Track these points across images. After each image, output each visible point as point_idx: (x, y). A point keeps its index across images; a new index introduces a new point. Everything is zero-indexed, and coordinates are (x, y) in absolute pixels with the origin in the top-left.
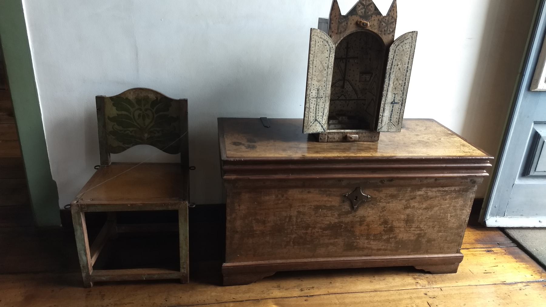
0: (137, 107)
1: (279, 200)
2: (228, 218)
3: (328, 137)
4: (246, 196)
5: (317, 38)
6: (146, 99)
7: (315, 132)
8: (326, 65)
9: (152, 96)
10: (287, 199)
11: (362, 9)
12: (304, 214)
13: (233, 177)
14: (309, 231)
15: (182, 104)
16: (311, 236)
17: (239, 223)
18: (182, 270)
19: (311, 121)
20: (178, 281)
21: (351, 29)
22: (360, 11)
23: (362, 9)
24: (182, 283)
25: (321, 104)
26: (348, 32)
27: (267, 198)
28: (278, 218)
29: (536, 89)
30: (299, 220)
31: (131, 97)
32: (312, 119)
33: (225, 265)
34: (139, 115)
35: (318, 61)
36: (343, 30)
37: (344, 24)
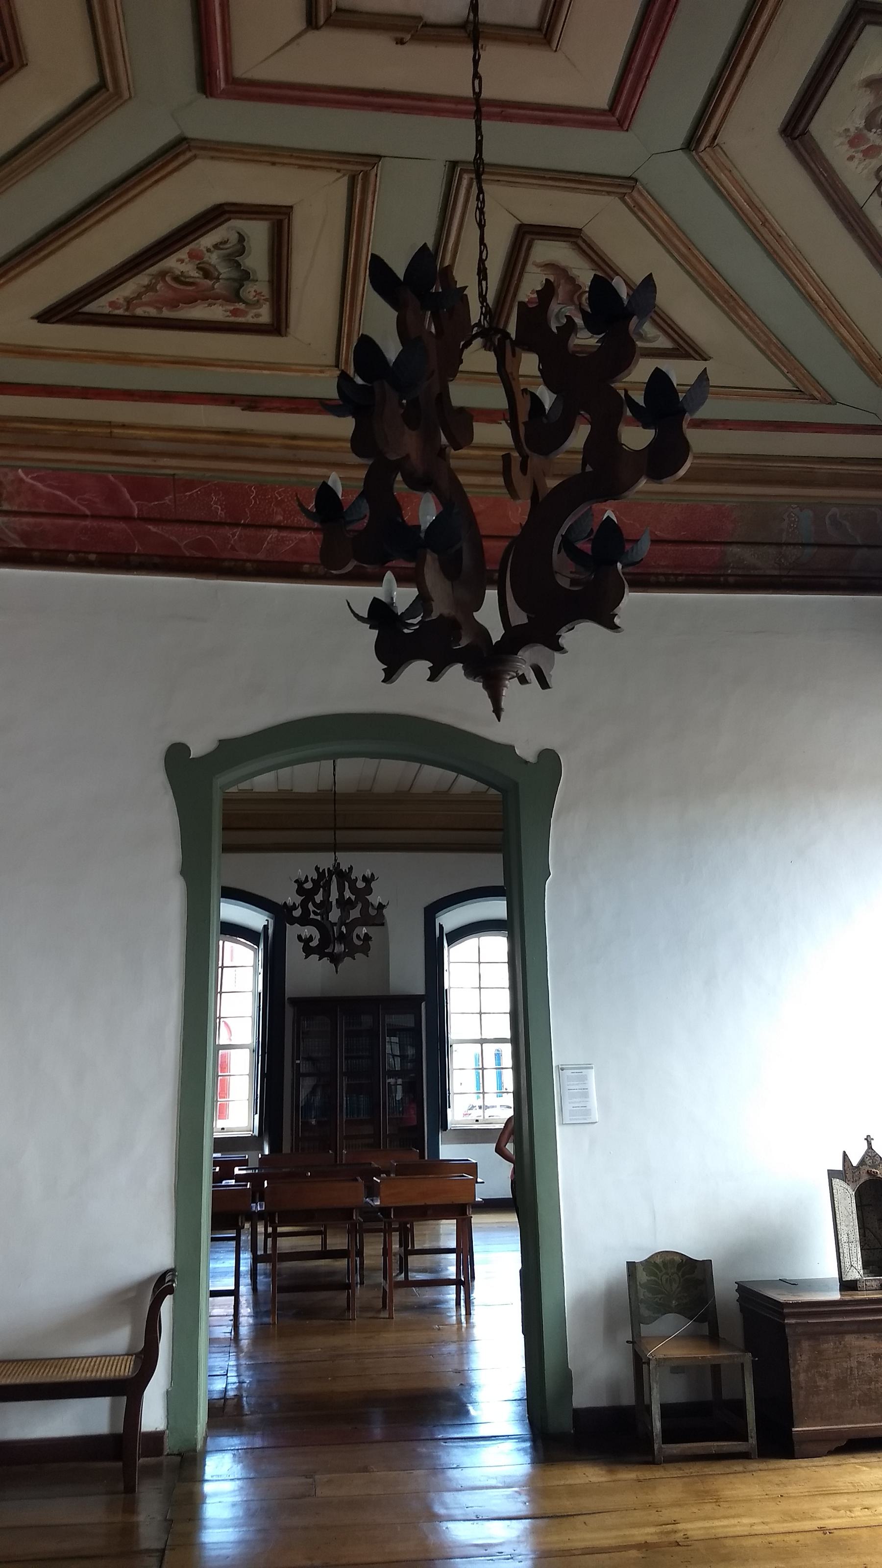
0: (664, 1271)
1: (838, 1348)
2: (792, 1370)
3: (866, 1284)
4: (805, 1344)
5: (838, 1187)
6: (672, 1262)
7: (853, 1279)
8: (851, 1210)
9: (677, 1258)
10: (845, 1346)
11: (869, 1160)
12: (864, 1364)
13: (793, 1321)
14: (872, 1386)
15: (706, 1265)
16: (876, 1392)
17: (802, 1377)
18: (750, 1440)
19: (848, 1266)
20: (744, 1456)
21: (865, 1178)
22: (869, 1162)
23: (869, 1160)
24: (751, 1459)
25: (853, 1248)
26: (862, 1181)
27: (826, 1346)
28: (840, 1371)
29: (565, 550)
30: (860, 1373)
31: (658, 1261)
32: (848, 1265)
33: (793, 1429)
34: (667, 1280)
35: (843, 1207)
36: (857, 1178)
37: (856, 1173)
